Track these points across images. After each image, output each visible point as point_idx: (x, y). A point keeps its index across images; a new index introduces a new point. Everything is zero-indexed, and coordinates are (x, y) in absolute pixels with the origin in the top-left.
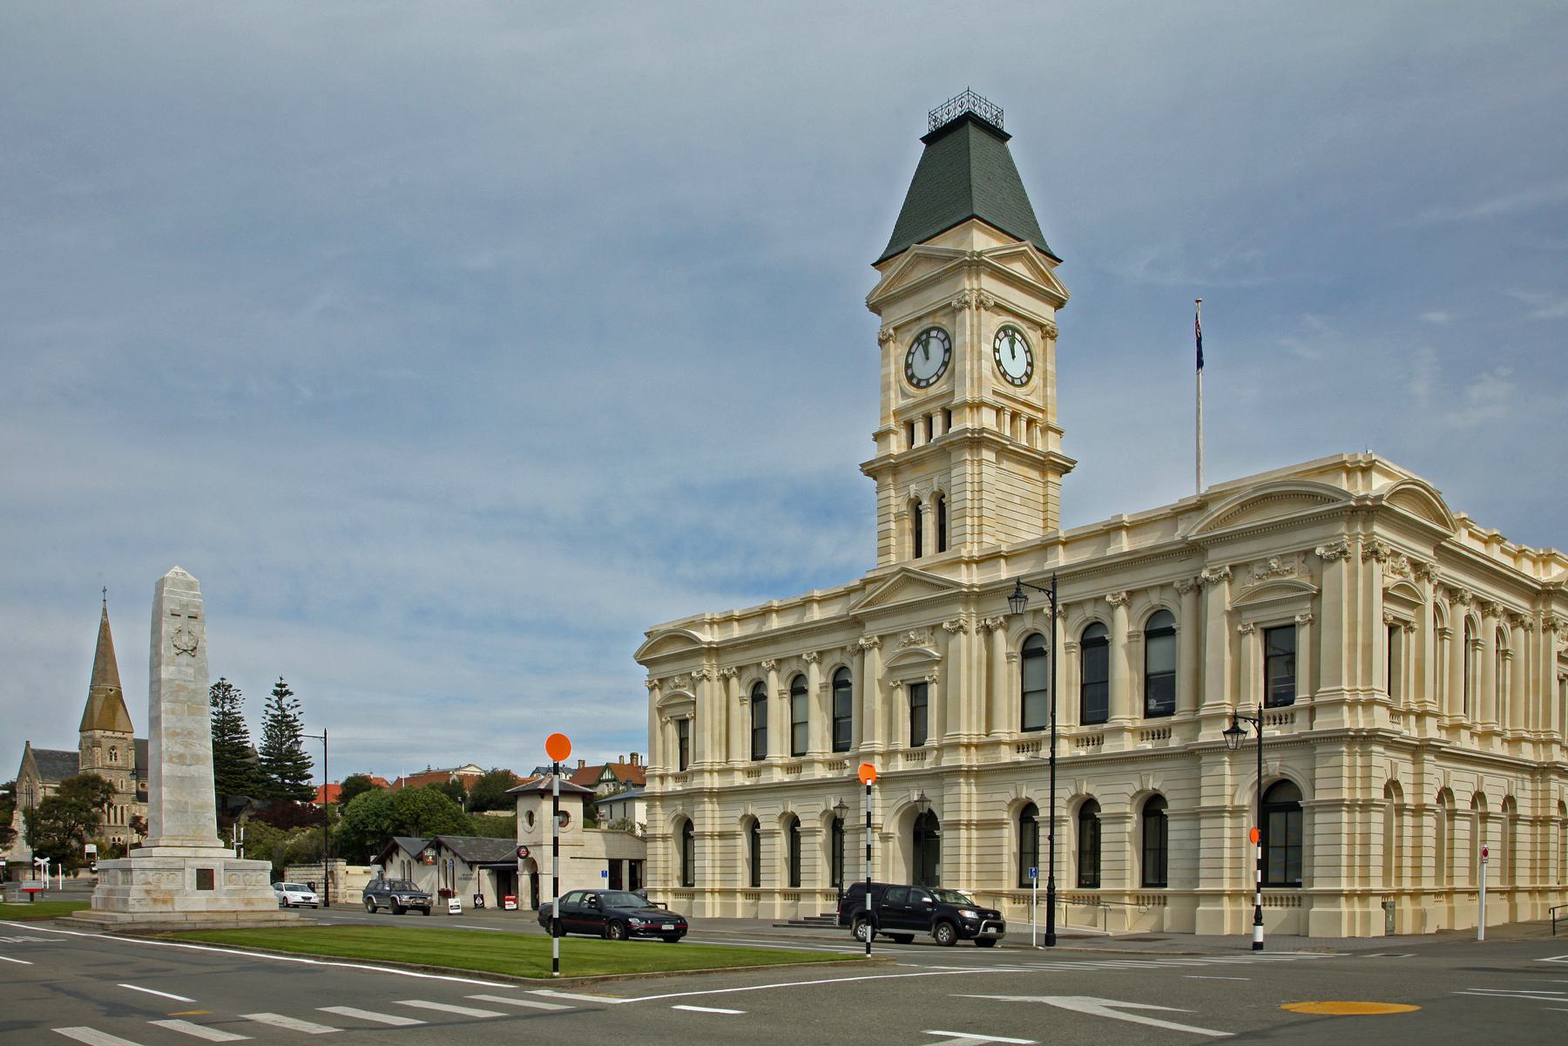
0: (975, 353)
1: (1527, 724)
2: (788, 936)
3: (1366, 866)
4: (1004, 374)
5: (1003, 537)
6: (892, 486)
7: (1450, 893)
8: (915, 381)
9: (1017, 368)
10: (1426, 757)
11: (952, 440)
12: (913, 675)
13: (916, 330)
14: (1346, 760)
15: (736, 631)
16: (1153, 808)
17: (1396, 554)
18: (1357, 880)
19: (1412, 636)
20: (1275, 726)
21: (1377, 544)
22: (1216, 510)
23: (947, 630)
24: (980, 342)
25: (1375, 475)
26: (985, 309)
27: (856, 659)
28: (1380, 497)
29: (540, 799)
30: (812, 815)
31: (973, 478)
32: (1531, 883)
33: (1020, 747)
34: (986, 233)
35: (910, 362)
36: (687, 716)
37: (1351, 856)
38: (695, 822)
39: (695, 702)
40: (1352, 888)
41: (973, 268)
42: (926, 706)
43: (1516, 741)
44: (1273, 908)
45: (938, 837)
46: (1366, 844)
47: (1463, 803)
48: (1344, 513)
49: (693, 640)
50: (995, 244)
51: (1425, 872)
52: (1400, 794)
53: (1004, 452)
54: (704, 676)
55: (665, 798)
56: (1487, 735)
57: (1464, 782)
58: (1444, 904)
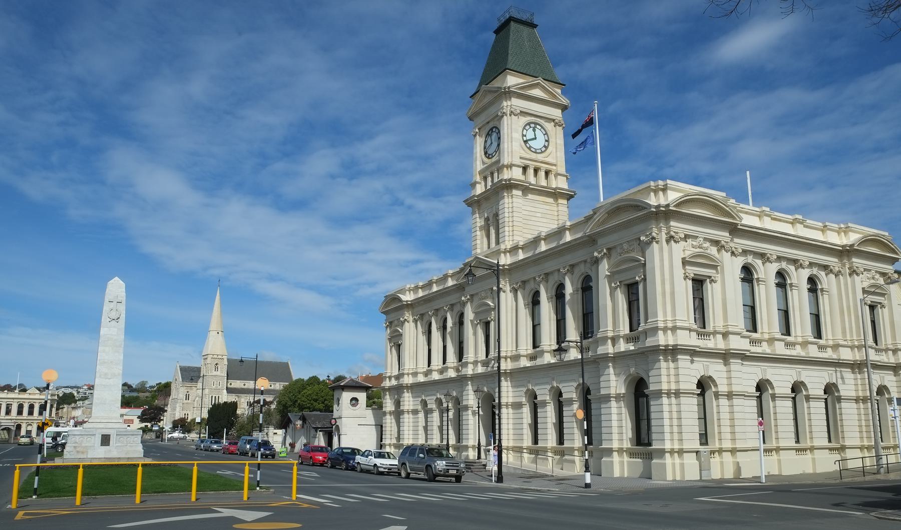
2: (873, 322)
8: (487, 155)
10: (731, 361)
11: (498, 185)
20: (633, 343)
22: (597, 218)
24: (512, 133)
25: (669, 192)
26: (514, 115)
32: (861, 442)
36: (637, 278)
39: (644, 265)
40: (734, 446)
48: (651, 215)
50: (521, 81)
53: (526, 190)
54: (405, 320)
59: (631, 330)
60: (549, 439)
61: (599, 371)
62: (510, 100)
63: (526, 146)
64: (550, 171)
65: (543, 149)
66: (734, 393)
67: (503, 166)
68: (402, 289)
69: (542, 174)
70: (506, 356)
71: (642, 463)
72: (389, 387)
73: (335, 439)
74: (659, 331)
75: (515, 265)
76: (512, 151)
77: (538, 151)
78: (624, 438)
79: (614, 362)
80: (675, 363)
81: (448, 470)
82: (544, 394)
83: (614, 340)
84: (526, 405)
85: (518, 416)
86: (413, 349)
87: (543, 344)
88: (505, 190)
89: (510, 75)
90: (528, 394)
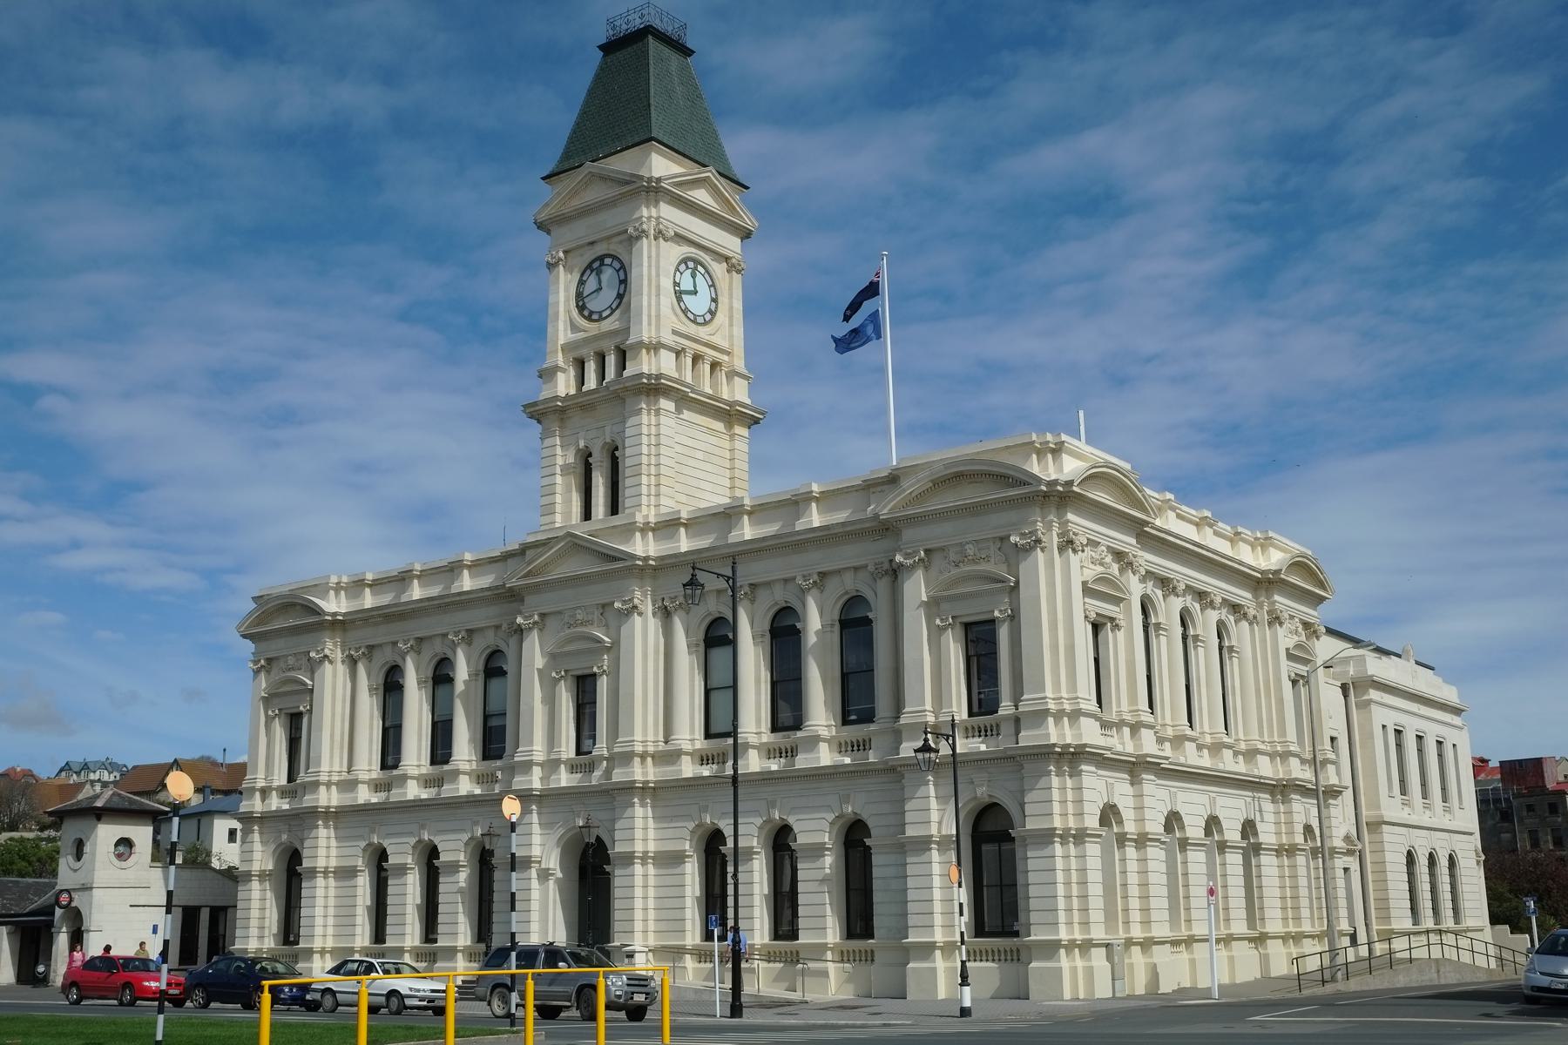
1: (1261, 734)
3: (1085, 910)
5: (683, 499)
7: (1190, 941)
8: (586, 313)
9: (699, 304)
11: (627, 385)
12: (580, 666)
13: (590, 255)
14: (1055, 781)
15: (369, 600)
16: (854, 838)
17: (1093, 544)
18: (1076, 926)
19: (1121, 635)
20: (981, 739)
21: (1071, 533)
22: (910, 486)
23: (619, 610)
24: (658, 275)
26: (664, 239)
27: (513, 641)
28: (1070, 483)
29: (95, 821)
30: (455, 850)
31: (649, 430)
33: (704, 759)
34: (665, 157)
36: (301, 708)
37: (1068, 897)
38: (305, 853)
39: (312, 690)
42: (595, 703)
43: (1251, 754)
44: (978, 964)
45: (608, 873)
46: (1083, 883)
47: (1195, 830)
49: (314, 610)
50: (680, 170)
51: (1154, 916)
52: (1120, 822)
53: (684, 400)
54: (326, 656)
55: (266, 819)
56: (1216, 748)
57: (1194, 804)
58: (1183, 955)
59: (578, 752)
60: (407, 932)
61: (903, 789)
65: (708, 317)
66: (1150, 836)
67: (640, 345)
68: (316, 585)
70: (329, 781)
71: (998, 971)
72: (261, 813)
74: (750, 750)
75: (673, 560)
78: (267, 933)
79: (540, 803)
80: (1074, 778)
81: (633, 993)
82: (402, 853)
83: (265, 792)
84: (363, 871)
85: (349, 892)
86: (341, 727)
87: (813, 723)
89: (657, 153)
90: (368, 853)
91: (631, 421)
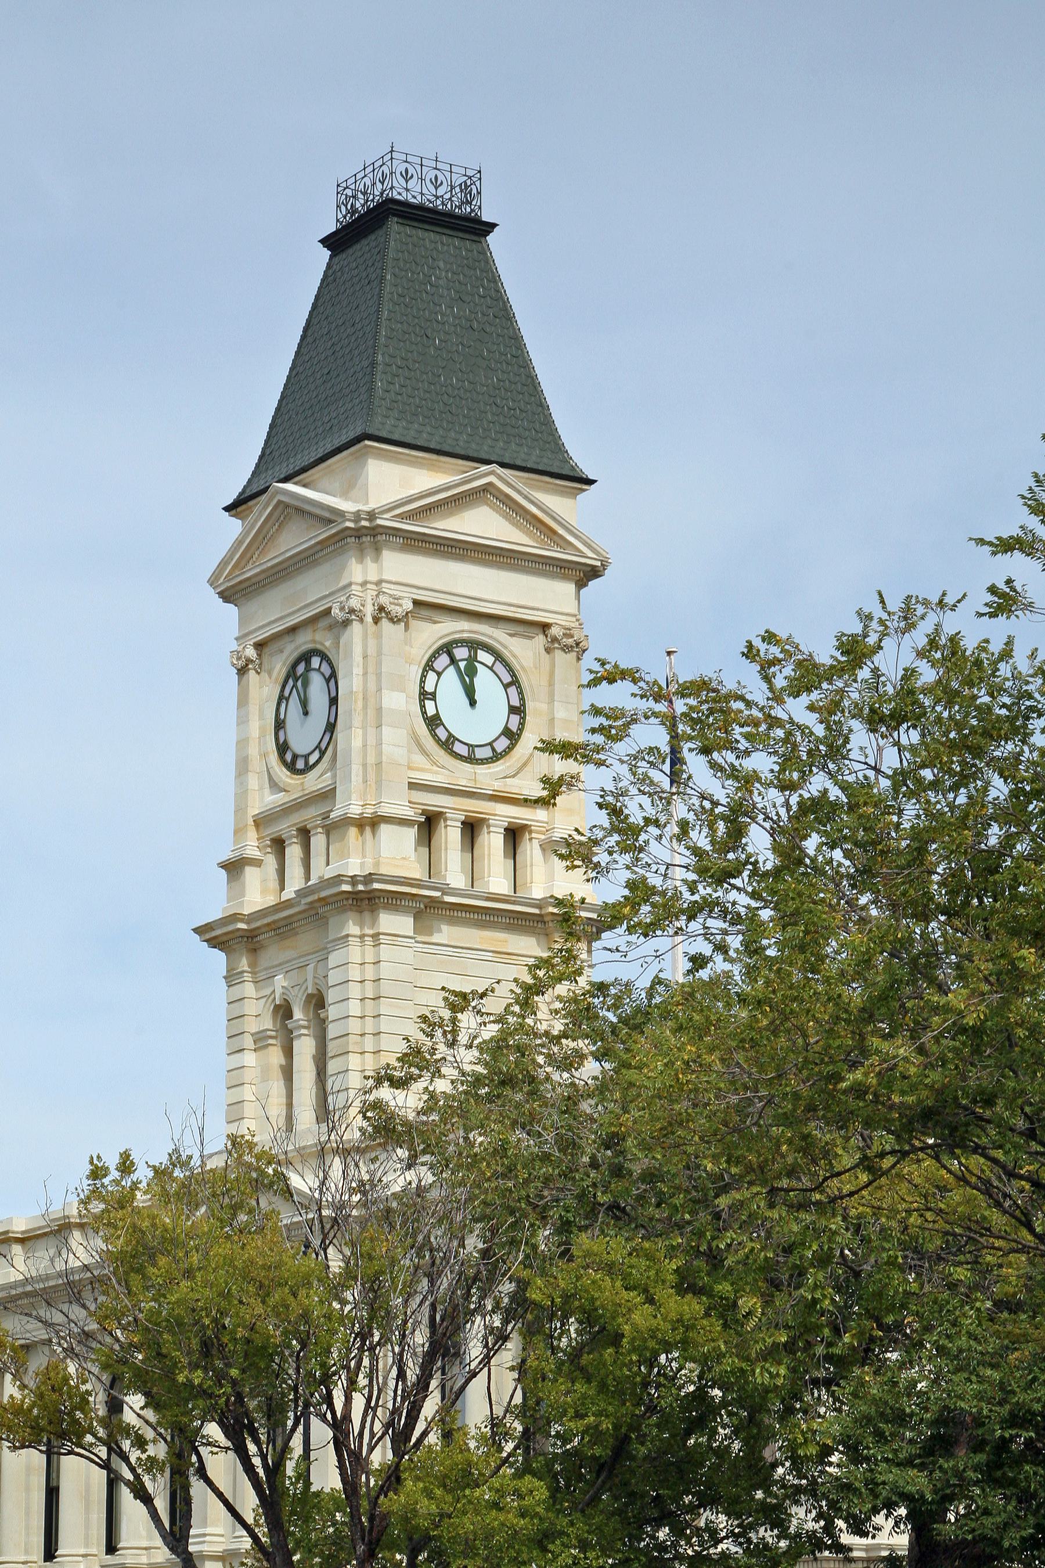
0: (371, 713)
4: (448, 744)
6: (247, 976)
11: (323, 894)
13: (292, 649)
24: (379, 690)
26: (391, 620)
35: (282, 716)
41: (364, 539)
62: (377, 558)
63: (435, 736)
64: (524, 828)
65: (502, 744)
69: (493, 841)
73: (269, 1033)
76: (379, 764)
77: (481, 754)
88: (351, 915)
91: (334, 959)
